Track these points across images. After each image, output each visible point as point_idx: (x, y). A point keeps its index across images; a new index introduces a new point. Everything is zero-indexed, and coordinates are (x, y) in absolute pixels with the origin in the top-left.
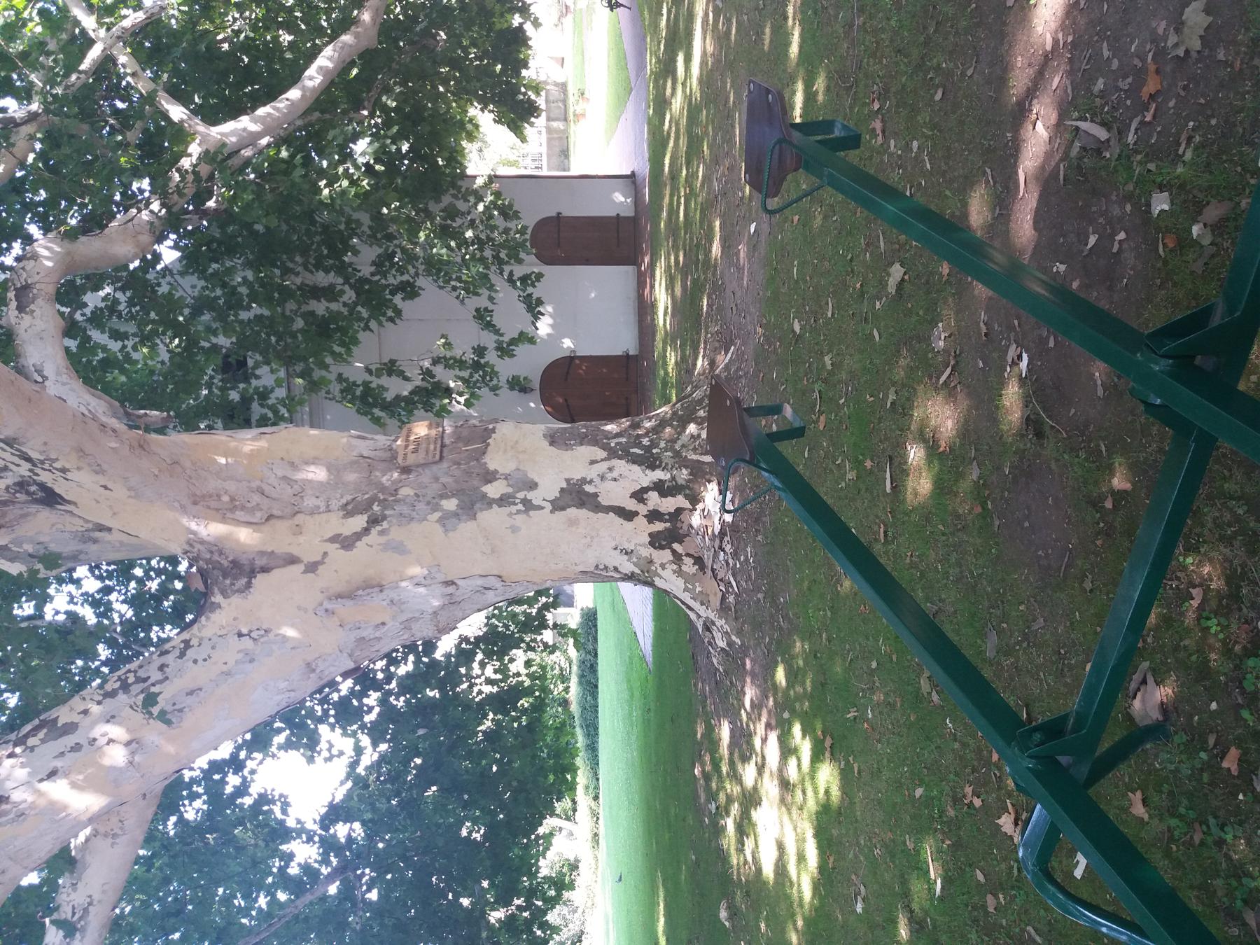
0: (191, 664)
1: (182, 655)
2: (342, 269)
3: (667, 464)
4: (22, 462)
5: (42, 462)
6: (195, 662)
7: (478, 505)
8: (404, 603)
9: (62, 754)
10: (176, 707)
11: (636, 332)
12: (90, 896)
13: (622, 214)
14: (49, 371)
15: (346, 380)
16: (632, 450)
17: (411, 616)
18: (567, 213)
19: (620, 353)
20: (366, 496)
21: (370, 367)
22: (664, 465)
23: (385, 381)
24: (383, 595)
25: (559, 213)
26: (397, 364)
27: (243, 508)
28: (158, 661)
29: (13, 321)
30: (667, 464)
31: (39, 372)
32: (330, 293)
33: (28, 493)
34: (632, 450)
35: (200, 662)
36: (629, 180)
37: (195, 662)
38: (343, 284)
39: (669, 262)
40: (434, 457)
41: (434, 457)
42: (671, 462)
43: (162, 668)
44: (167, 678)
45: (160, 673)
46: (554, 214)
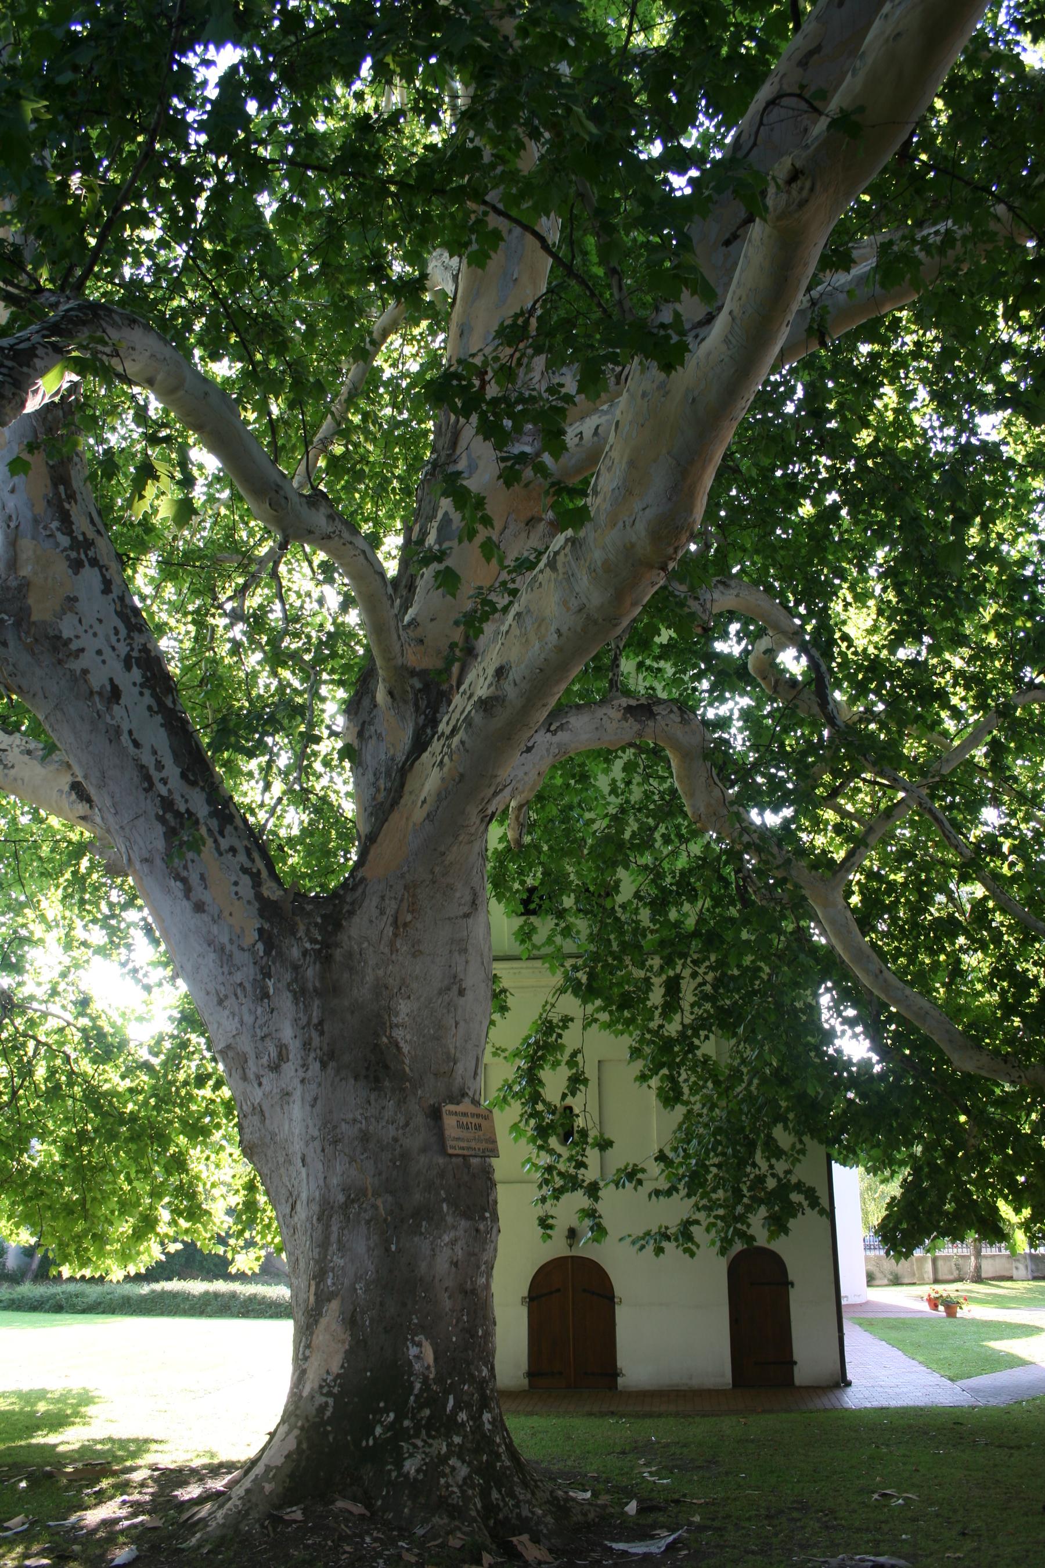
0: (234, 878)
1: (245, 870)
2: (701, 1024)
3: (430, 1446)
4: (450, 727)
5: (449, 746)
6: (236, 884)
7: (390, 1199)
8: (282, 1108)
9: (155, 753)
10: (190, 863)
11: (648, 1388)
12: (13, 767)
13: (796, 1369)
14: (562, 736)
15: (565, 1027)
16: (451, 1397)
17: (267, 1115)
18: (794, 1294)
19: (619, 1364)
20: (407, 1069)
21: (579, 1056)
22: (430, 1441)
23: (564, 1072)
24: (296, 1082)
25: (792, 1284)
26: (582, 1087)
27: (395, 935)
28: (239, 845)
29: (615, 702)
30: (430, 1446)
31: (561, 727)
32: (671, 1006)
33: (425, 726)
34: (451, 1397)
35: (234, 889)
36: (839, 1378)
37: (236, 884)
38: (682, 1023)
39: (1013, 1299)
40: (454, 1148)
41: (454, 1148)
42: (433, 1451)
43: (233, 850)
44: (221, 854)
45: (227, 847)
46: (791, 1278)
